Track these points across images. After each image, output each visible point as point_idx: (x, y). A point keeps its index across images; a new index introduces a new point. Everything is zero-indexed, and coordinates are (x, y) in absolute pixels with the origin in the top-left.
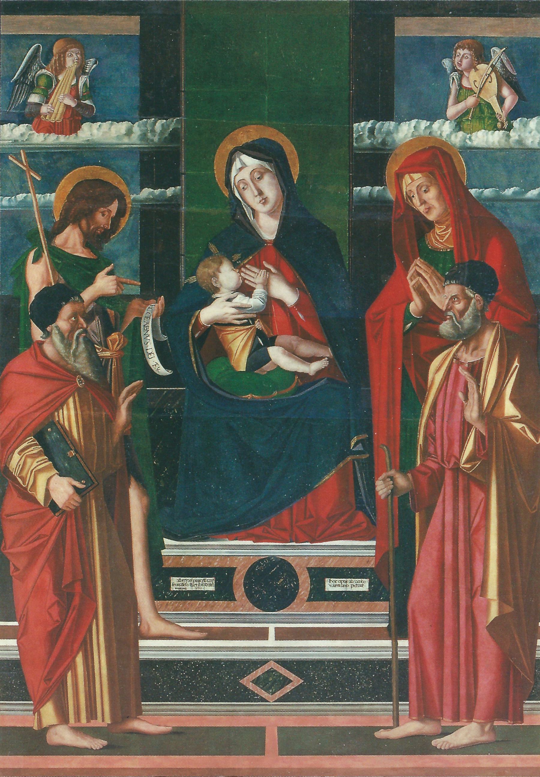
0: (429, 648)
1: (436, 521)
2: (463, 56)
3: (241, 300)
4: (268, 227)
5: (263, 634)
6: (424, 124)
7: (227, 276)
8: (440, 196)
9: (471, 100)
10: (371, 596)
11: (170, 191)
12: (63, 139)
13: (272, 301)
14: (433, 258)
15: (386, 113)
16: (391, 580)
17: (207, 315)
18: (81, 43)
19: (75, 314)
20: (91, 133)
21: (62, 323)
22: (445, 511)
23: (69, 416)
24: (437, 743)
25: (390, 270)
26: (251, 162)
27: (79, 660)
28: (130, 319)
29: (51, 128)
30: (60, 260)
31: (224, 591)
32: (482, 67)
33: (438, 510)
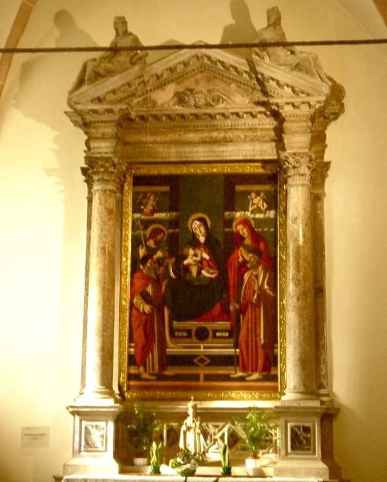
0: (245, 352)
1: (246, 317)
2: (253, 195)
3: (195, 258)
4: (202, 239)
5: (200, 348)
6: (243, 213)
7: (191, 252)
8: (247, 231)
9: (255, 206)
10: (230, 336)
11: (177, 230)
12: (149, 217)
13: (203, 259)
14: (246, 247)
15: (233, 209)
16: (234, 333)
17: (186, 262)
18: (155, 193)
19: (152, 263)
20: (157, 215)
21: (148, 265)
22: (249, 313)
23: (150, 289)
24: (247, 379)
25: (234, 251)
26: (198, 223)
27: (150, 355)
28: (166, 264)
29: (147, 215)
30: (148, 248)
31: (189, 336)
32: (258, 198)
33: (247, 314)
